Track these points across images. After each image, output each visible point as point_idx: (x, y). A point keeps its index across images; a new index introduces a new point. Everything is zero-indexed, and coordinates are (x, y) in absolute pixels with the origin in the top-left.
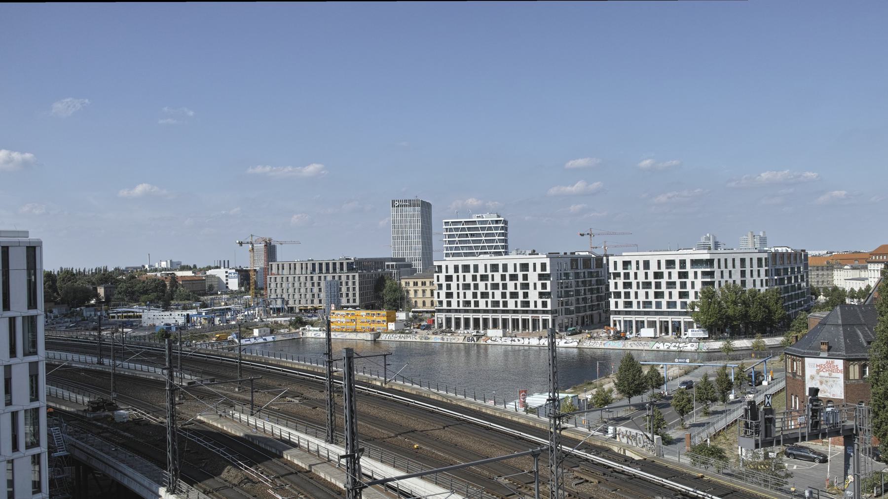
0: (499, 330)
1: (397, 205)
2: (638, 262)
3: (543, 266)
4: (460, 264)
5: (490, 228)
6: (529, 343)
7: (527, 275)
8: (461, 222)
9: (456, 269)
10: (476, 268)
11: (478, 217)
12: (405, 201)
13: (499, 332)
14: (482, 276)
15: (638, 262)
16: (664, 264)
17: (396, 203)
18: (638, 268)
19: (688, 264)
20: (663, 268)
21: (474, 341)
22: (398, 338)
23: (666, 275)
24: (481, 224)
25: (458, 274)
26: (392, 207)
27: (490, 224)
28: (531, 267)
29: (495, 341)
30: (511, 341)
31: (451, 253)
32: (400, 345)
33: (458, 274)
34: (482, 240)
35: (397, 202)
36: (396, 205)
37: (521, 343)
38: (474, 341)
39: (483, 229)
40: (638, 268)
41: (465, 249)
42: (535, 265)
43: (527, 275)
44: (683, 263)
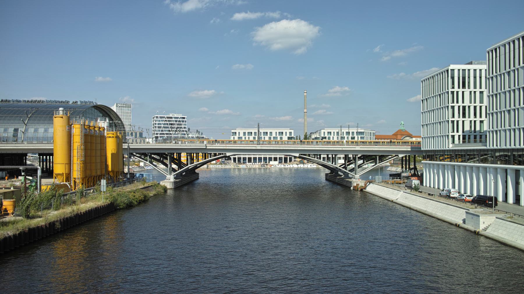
0: (116, 170)
1: (119, 106)
2: (334, 132)
3: (290, 133)
4: (247, 132)
5: (180, 121)
6: (293, 167)
7: (282, 137)
8: (165, 117)
9: (244, 133)
10: (271, 133)
11: (172, 115)
12: (124, 104)
13: (277, 162)
14: (274, 137)
15: (334, 132)
16: (345, 133)
17: (118, 105)
18: (334, 135)
19: (355, 134)
20: (345, 135)
21: (265, 167)
22: (221, 167)
23: (346, 138)
24: (175, 119)
25: (245, 136)
26: (116, 107)
27: (179, 119)
28: (284, 134)
29: (275, 166)
30: (284, 166)
31: (159, 133)
32: (382, 160)
33: (245, 136)
34: (161, 127)
35: (119, 105)
36: (118, 106)
37: (289, 166)
38: (265, 167)
39: (176, 121)
40: (334, 135)
41: (166, 131)
42: (286, 133)
43: (282, 137)
44: (353, 133)
